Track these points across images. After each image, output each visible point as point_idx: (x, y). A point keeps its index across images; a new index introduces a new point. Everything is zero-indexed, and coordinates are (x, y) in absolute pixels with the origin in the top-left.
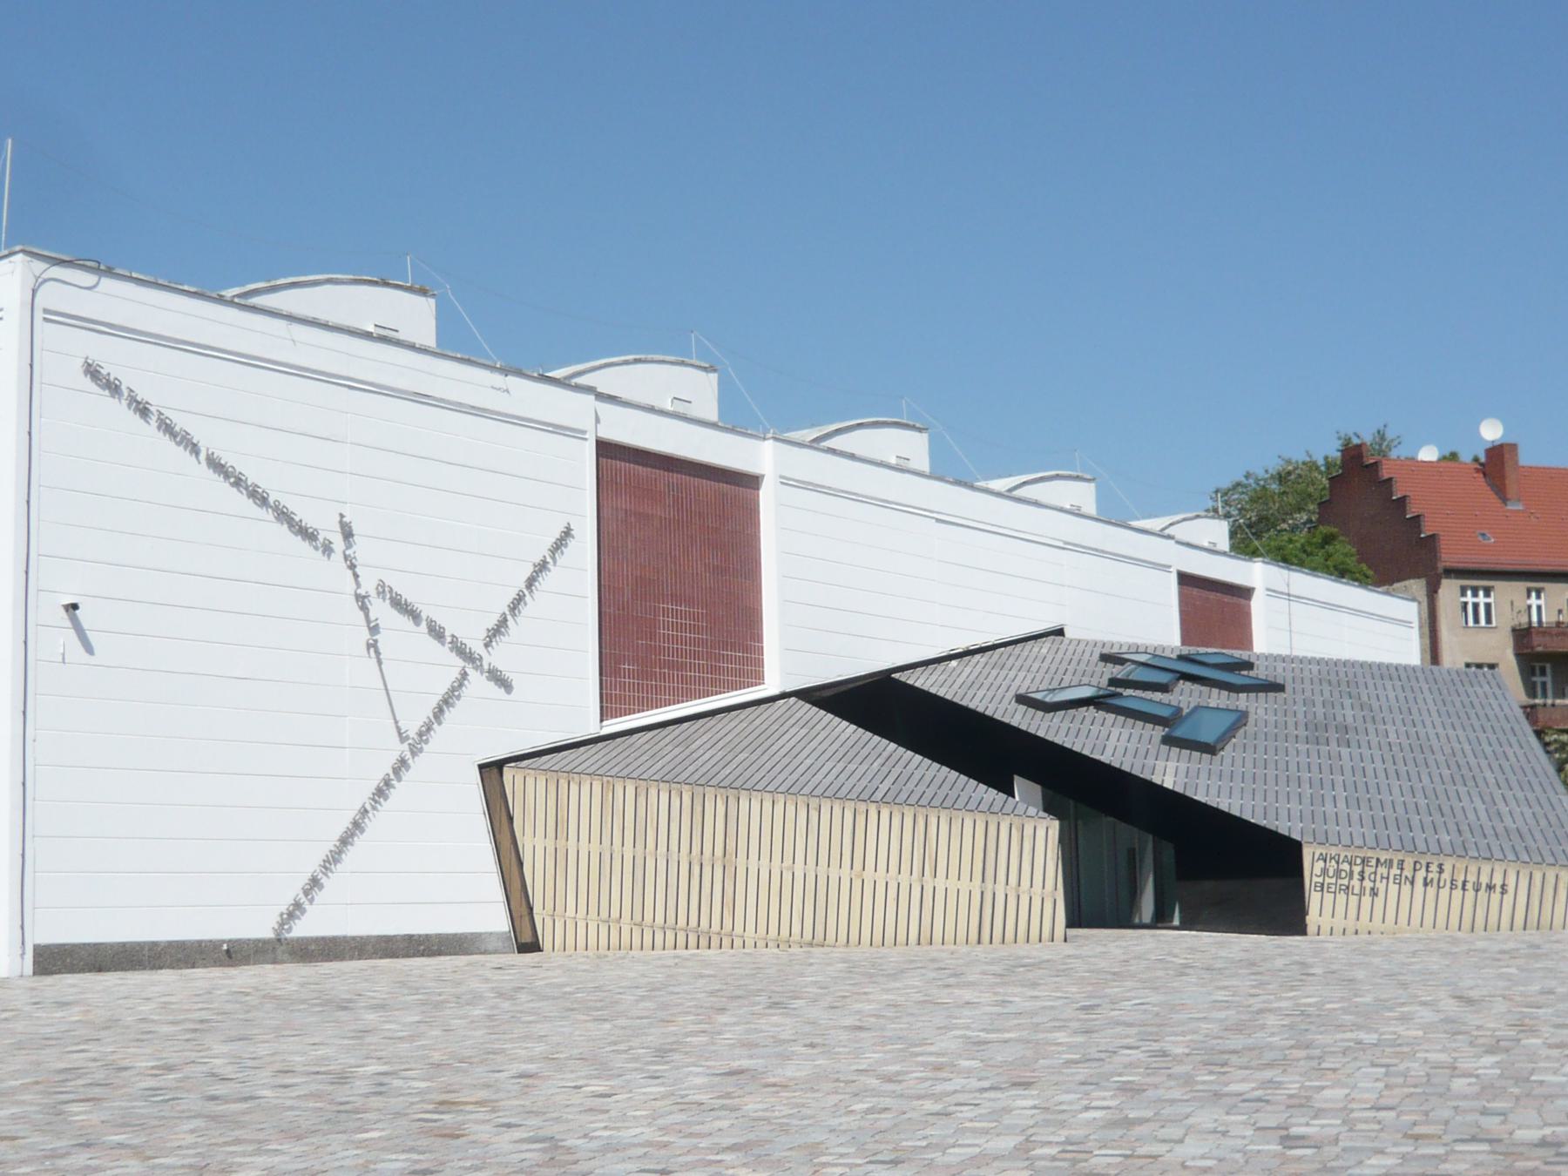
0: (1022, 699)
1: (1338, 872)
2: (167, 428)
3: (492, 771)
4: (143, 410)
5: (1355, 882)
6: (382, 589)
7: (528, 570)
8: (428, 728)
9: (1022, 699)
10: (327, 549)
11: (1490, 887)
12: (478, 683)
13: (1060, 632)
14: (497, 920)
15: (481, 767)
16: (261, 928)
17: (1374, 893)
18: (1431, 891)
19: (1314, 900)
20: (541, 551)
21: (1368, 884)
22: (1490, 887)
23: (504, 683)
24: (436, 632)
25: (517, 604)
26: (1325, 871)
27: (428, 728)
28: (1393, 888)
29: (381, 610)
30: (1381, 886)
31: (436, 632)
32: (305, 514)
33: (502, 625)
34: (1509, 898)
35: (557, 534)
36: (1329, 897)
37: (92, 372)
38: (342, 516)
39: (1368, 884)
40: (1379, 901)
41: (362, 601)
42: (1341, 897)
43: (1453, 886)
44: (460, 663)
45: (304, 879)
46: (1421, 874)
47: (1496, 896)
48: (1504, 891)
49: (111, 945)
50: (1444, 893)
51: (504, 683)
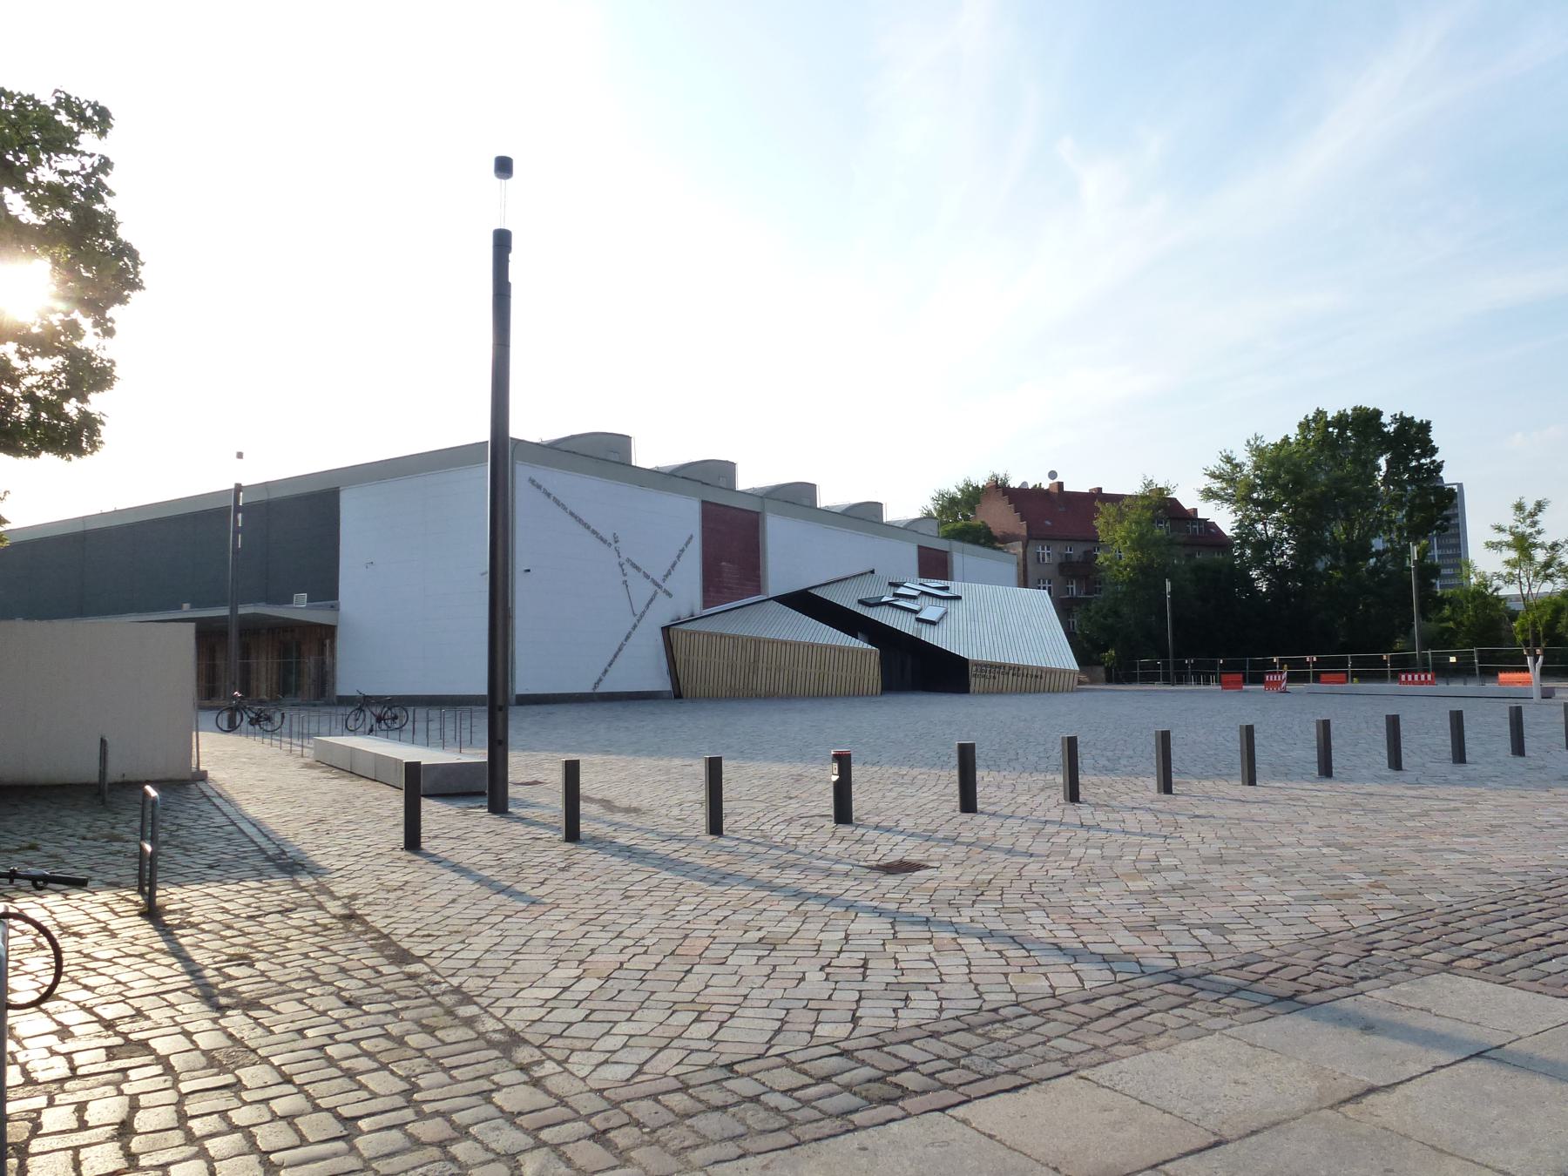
3: (666, 630)
6: (628, 560)
12: (660, 594)
14: (668, 687)
16: (585, 687)
19: (972, 680)
23: (670, 595)
29: (627, 567)
31: (647, 577)
32: (602, 533)
33: (669, 573)
37: (532, 481)
41: (621, 565)
51: (670, 595)
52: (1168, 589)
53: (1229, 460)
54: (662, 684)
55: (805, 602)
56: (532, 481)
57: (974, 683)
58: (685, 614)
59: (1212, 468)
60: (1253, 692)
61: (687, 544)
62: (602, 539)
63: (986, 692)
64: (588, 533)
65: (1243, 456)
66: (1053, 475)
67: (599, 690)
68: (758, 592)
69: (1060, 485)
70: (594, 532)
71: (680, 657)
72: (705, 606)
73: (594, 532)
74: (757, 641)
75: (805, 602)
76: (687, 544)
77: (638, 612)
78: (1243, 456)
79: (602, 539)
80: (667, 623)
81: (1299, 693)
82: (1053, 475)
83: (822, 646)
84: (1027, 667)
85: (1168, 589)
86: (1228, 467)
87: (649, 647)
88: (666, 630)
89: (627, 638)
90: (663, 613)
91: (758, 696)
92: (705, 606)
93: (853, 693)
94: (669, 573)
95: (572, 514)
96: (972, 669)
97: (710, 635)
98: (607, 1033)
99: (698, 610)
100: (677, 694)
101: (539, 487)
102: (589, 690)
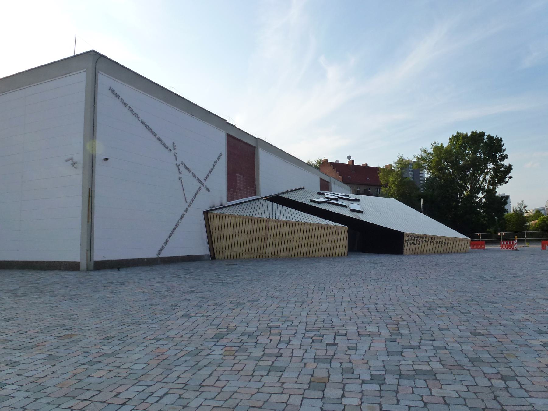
0: (359, 200)
1: (412, 239)
2: (132, 111)
3: (206, 213)
4: (125, 104)
5: (415, 242)
6: (182, 163)
7: (213, 163)
8: (192, 201)
9: (359, 200)
10: (170, 150)
11: (445, 243)
12: (203, 190)
13: (304, 188)
14: (207, 252)
15: (204, 212)
16: (153, 254)
17: (419, 244)
18: (432, 244)
19: (406, 246)
20: (215, 159)
21: (418, 242)
22: (445, 243)
23: (208, 190)
24: (194, 176)
25: (210, 172)
26: (408, 239)
27: (192, 201)
28: (424, 243)
29: (182, 168)
30: (421, 243)
31: (194, 176)
32: (165, 141)
33: (208, 176)
34: (449, 245)
35: (218, 155)
36: (409, 245)
37: (113, 91)
38: (174, 143)
39: (418, 242)
40: (420, 246)
41: (178, 166)
42: (412, 245)
43: (437, 243)
44: (200, 185)
45: (164, 241)
46: (430, 240)
47: (446, 245)
48: (448, 244)
49: (116, 260)
50: (435, 244)
51: (208, 190)
52: (422, 202)
53: (425, 152)
54: (203, 250)
55: (277, 199)
56: (113, 91)
57: (407, 247)
58: (217, 205)
59: (417, 155)
60: (494, 251)
61: (219, 158)
62: (165, 145)
63: (415, 254)
64: (155, 139)
65: (430, 151)
66: (349, 157)
67: (162, 255)
68: (255, 194)
69: (353, 161)
70: (159, 139)
71: (215, 232)
72: (229, 200)
73: (159, 139)
74: (268, 221)
75: (277, 199)
76: (219, 158)
77: (189, 200)
78: (430, 151)
79: (165, 145)
80: (207, 209)
81: (494, 251)
82: (349, 157)
83: (308, 223)
84: (440, 237)
85: (422, 202)
86: (424, 155)
87: (195, 226)
88: (206, 213)
89: (182, 218)
90: (205, 202)
91: (267, 259)
92: (229, 200)
93: (330, 256)
94: (208, 176)
95: (143, 123)
96: (406, 239)
97: (235, 217)
98: (136, 406)
99: (225, 203)
100: (213, 257)
101: (118, 96)
102: (155, 256)
